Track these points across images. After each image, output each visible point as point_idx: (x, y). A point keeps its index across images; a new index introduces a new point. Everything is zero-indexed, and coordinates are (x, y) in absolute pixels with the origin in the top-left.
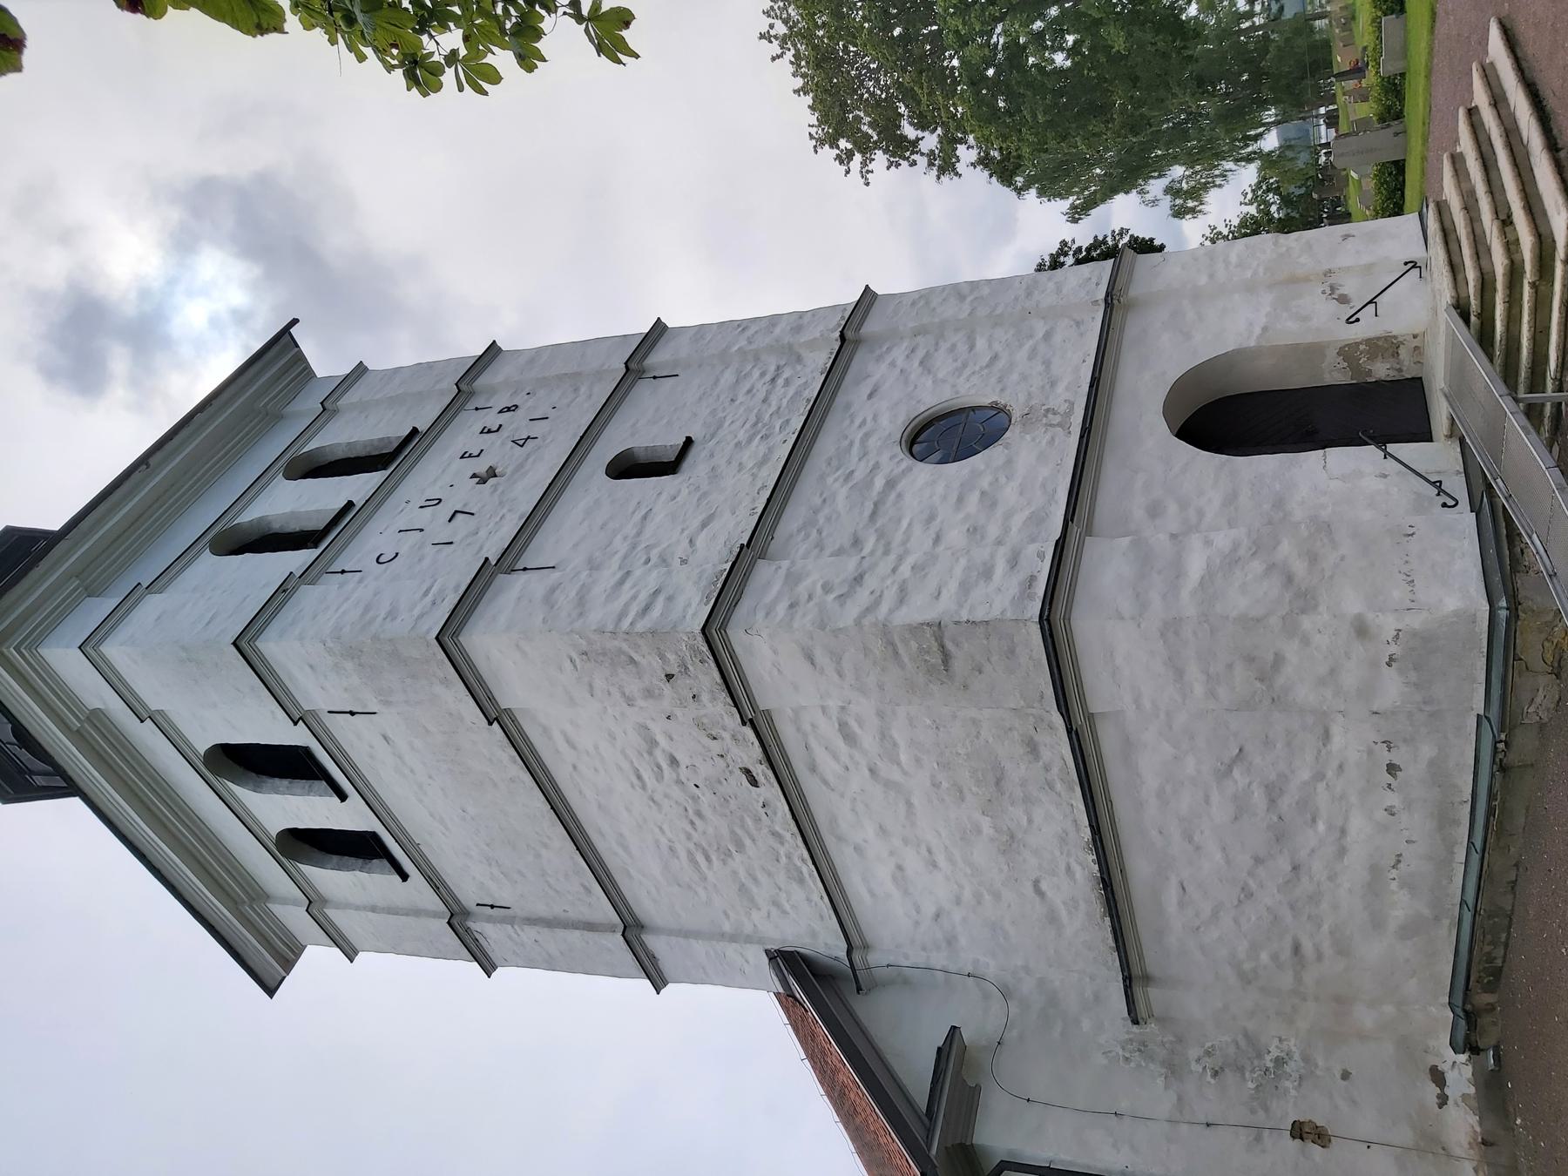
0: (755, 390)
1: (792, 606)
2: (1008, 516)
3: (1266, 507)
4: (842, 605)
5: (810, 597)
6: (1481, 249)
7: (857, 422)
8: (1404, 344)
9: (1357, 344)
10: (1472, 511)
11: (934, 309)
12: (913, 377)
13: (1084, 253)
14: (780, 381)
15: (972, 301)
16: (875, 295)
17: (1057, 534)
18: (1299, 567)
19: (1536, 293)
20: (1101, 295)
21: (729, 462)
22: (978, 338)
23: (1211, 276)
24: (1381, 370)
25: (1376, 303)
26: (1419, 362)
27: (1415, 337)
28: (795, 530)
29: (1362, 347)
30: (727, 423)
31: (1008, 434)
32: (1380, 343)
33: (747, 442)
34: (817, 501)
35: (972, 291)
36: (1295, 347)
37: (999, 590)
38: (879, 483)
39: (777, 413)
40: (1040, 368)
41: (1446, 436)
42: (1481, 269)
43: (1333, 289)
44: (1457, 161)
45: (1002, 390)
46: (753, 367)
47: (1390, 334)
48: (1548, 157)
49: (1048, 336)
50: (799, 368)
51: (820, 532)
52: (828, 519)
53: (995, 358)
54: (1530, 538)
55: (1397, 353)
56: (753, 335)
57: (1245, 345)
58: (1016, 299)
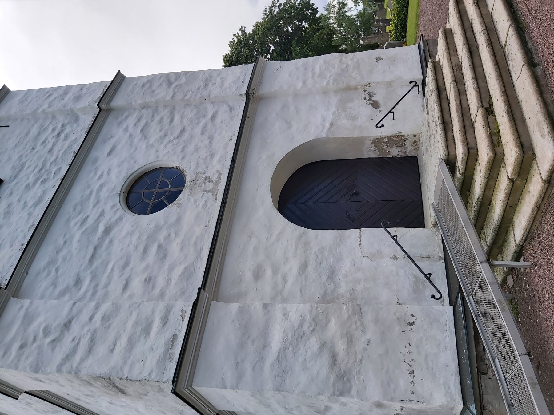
0: (47, 142)
1: (22, 347)
2: (171, 269)
3: (324, 278)
4: (53, 349)
5: (35, 339)
6: (467, 123)
7: (99, 173)
8: (408, 140)
9: (382, 139)
10: (450, 305)
11: (154, 91)
12: (136, 140)
13: (282, 6)
14: (63, 136)
15: (175, 87)
16: (123, 77)
17: (194, 298)
18: (341, 346)
19: (513, 185)
20: (244, 91)
21: (19, 200)
22: (176, 114)
23: (304, 83)
24: (395, 152)
25: (393, 112)
26: (416, 149)
27: (415, 136)
28: (42, 268)
29: (385, 140)
30: (26, 167)
31: (181, 196)
32: (395, 139)
33: (33, 184)
34: (61, 241)
35: (176, 80)
36: (347, 139)
37: (152, 348)
38: (101, 228)
39: (55, 162)
40: (207, 142)
41: (433, 225)
42: (467, 144)
43: (370, 95)
44: (448, 35)
45: (183, 158)
46: (50, 123)
47: (401, 134)
48: (529, 74)
49: (213, 117)
50: (75, 126)
51: (57, 270)
52: (64, 259)
53: (183, 131)
54: (494, 361)
55: (404, 144)
56: (53, 101)
57: (320, 137)
58: (199, 88)
